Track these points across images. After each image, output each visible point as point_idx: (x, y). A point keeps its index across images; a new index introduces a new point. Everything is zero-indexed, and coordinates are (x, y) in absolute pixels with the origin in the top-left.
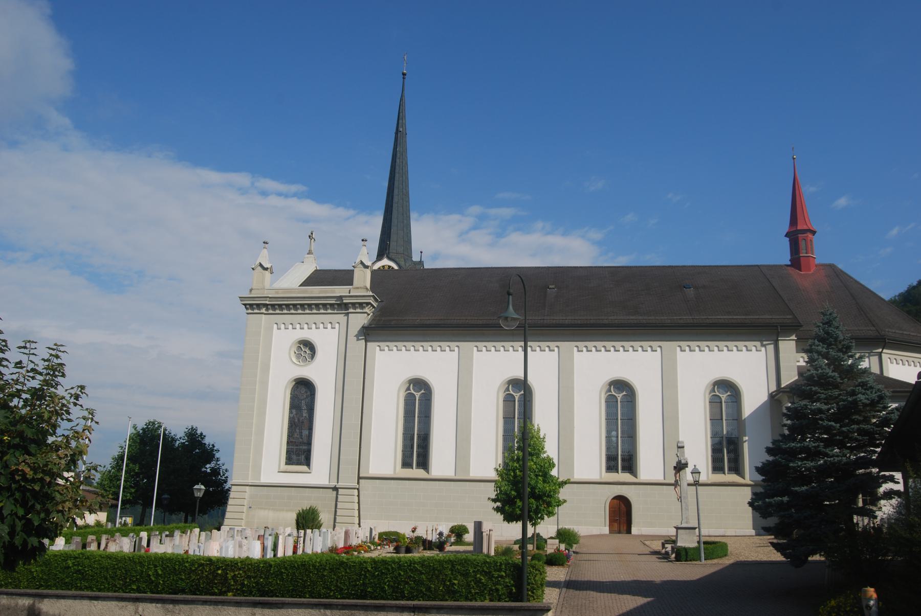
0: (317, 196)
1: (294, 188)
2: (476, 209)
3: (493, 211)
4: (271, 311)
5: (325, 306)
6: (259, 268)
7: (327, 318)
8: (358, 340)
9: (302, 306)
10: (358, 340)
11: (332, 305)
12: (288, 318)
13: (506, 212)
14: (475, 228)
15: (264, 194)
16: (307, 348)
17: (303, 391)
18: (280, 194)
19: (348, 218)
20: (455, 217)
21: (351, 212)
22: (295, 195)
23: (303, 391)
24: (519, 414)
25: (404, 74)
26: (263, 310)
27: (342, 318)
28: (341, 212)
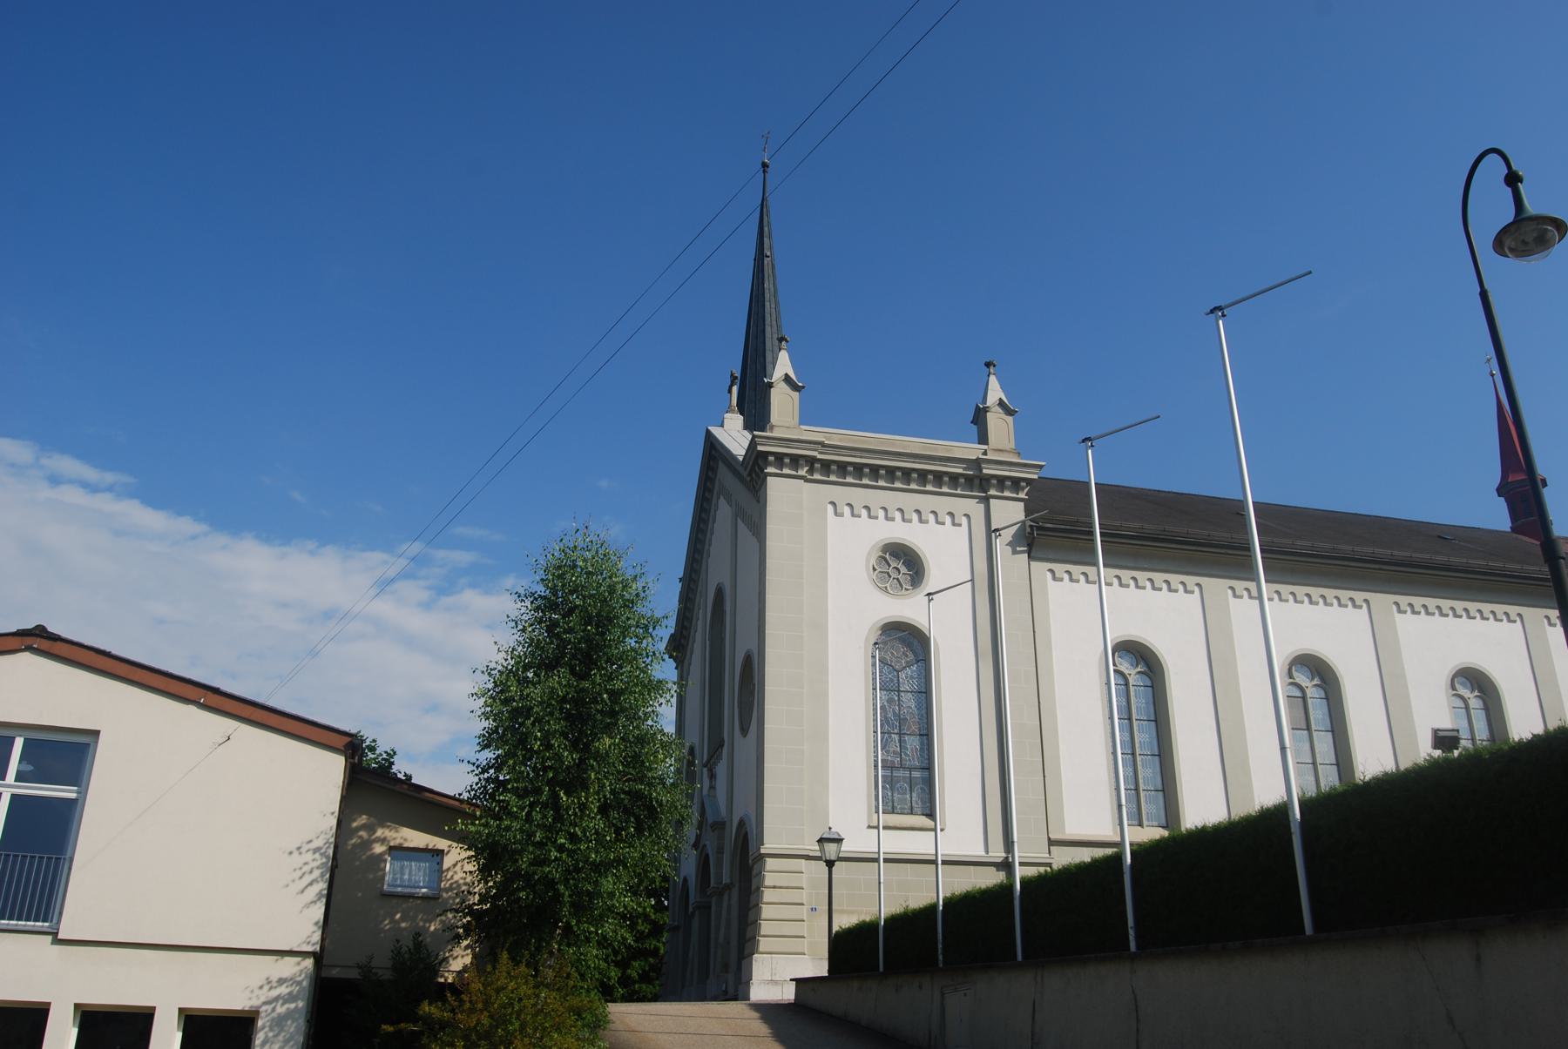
0: (153, 497)
1: (110, 477)
2: (417, 547)
3: (441, 554)
4: (817, 476)
5: (939, 478)
6: (784, 385)
7: (943, 504)
8: (1015, 552)
9: (907, 474)
10: (1015, 552)
11: (954, 479)
12: (859, 496)
13: (463, 557)
14: (405, 575)
15: (55, 480)
16: (903, 564)
17: (905, 645)
18: (86, 485)
19: (194, 537)
20: (377, 556)
21: (200, 528)
22: (110, 489)
23: (905, 645)
24: (1292, 719)
25: (765, 165)
26: (803, 472)
27: (974, 507)
28: (187, 525)
